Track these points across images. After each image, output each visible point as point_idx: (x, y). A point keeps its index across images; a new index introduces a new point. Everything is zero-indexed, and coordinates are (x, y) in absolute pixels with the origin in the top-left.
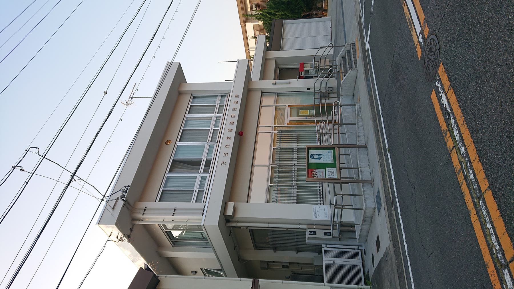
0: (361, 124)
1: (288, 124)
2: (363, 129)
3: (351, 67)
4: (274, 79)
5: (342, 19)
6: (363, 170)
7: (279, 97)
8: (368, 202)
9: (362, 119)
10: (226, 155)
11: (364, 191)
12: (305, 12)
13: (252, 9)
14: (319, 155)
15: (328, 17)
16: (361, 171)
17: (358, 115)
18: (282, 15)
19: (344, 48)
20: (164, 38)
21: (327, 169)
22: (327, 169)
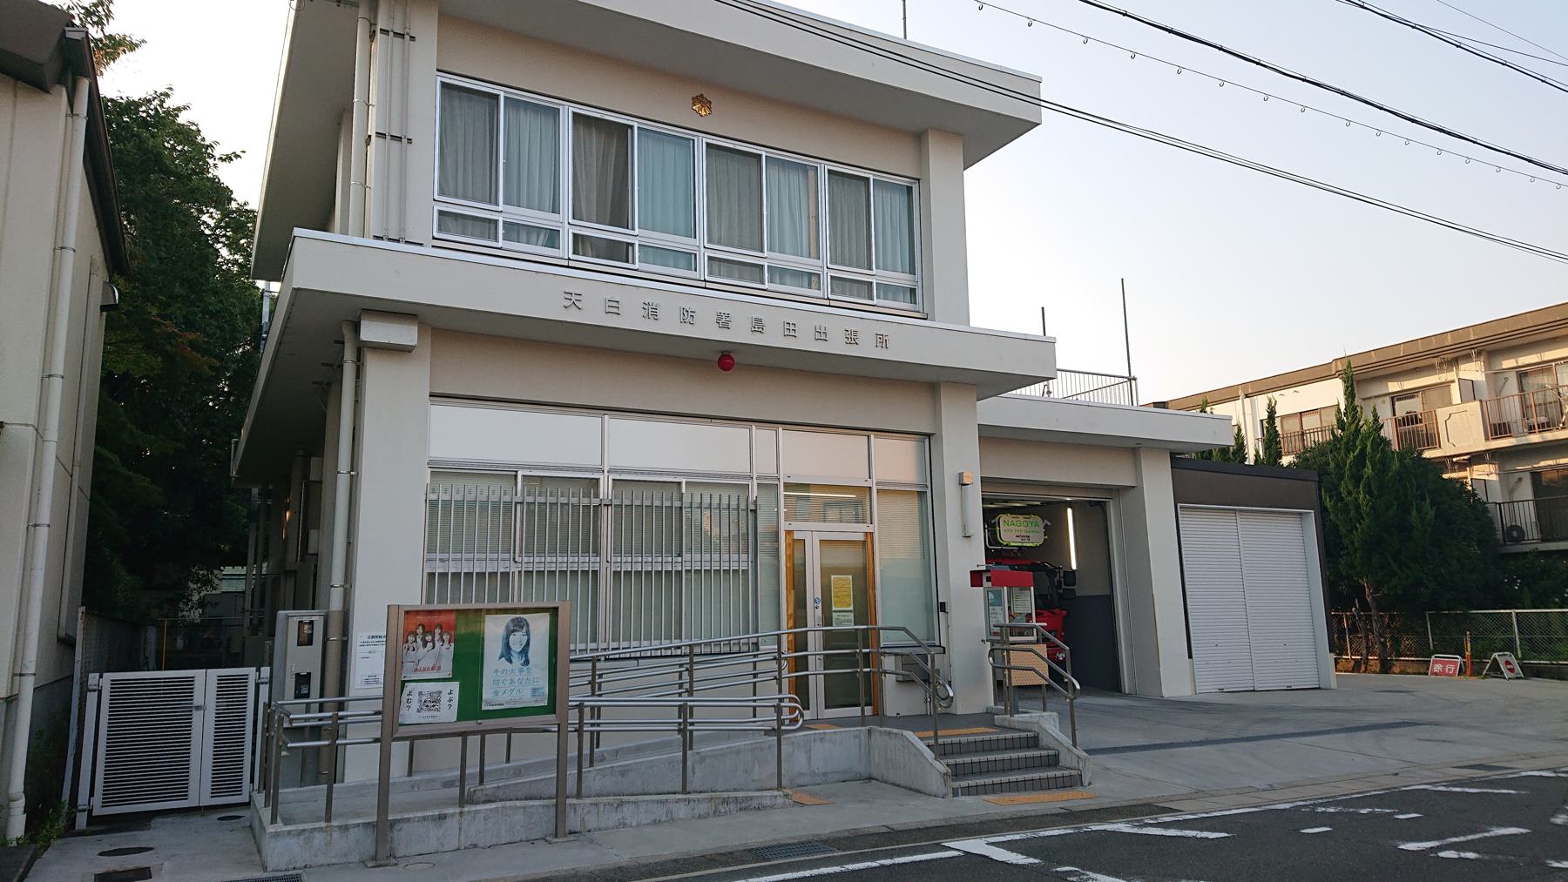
0: (682, 811)
1: (789, 533)
2: (656, 822)
3: (957, 772)
4: (985, 481)
5: (1279, 729)
6: (452, 824)
7: (915, 501)
8: (295, 844)
9: (707, 816)
10: (758, 326)
11: (346, 828)
12: (1376, 590)
13: (1396, 397)
14: (525, 651)
15: (1332, 677)
16: (442, 817)
17: (725, 801)
18: (1358, 507)
19: (1068, 742)
20: (1086, 40)
21: (455, 686)
22: (455, 686)
